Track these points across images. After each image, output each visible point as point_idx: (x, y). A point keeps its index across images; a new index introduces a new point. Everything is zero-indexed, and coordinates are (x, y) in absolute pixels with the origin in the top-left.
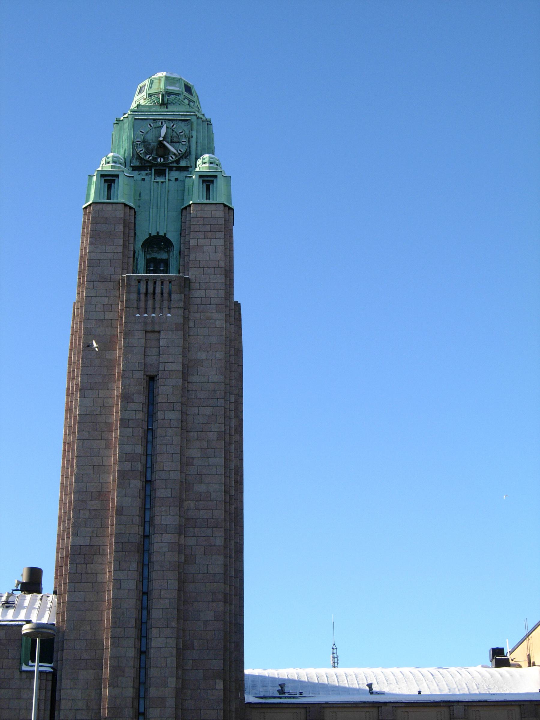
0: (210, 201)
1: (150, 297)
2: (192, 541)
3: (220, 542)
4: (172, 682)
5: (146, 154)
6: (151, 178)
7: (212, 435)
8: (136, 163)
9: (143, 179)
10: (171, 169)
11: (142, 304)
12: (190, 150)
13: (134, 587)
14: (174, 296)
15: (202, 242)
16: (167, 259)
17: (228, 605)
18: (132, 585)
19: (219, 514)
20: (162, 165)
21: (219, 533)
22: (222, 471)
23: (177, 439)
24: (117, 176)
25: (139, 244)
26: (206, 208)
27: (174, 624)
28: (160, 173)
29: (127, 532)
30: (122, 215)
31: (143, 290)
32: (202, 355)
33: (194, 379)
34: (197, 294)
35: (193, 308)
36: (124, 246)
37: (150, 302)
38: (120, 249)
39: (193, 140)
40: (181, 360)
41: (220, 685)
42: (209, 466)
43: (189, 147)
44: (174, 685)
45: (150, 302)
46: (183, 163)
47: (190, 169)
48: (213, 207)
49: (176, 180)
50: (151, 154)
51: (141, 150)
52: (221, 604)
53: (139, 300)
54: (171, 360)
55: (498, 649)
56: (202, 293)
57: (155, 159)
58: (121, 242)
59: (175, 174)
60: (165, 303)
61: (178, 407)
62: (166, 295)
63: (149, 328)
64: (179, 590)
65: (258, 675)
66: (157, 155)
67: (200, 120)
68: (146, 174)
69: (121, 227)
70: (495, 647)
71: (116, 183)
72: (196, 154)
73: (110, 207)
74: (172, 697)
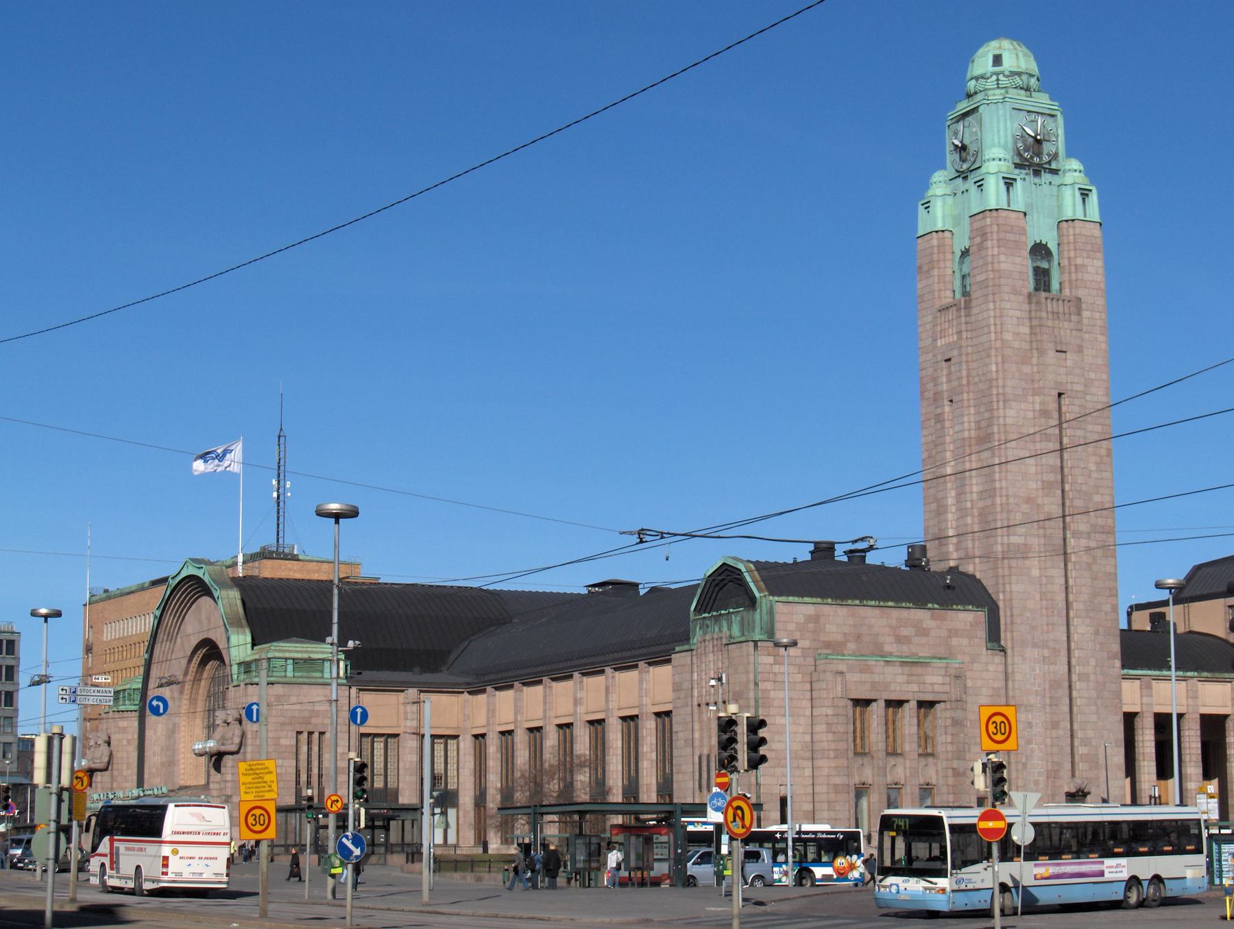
8: (1017, 161)
16: (990, 909)
20: (1038, 165)
43: (1057, 148)
50: (1028, 151)
57: (1032, 158)
65: (1225, 754)
66: (1033, 153)
74: (821, 741)
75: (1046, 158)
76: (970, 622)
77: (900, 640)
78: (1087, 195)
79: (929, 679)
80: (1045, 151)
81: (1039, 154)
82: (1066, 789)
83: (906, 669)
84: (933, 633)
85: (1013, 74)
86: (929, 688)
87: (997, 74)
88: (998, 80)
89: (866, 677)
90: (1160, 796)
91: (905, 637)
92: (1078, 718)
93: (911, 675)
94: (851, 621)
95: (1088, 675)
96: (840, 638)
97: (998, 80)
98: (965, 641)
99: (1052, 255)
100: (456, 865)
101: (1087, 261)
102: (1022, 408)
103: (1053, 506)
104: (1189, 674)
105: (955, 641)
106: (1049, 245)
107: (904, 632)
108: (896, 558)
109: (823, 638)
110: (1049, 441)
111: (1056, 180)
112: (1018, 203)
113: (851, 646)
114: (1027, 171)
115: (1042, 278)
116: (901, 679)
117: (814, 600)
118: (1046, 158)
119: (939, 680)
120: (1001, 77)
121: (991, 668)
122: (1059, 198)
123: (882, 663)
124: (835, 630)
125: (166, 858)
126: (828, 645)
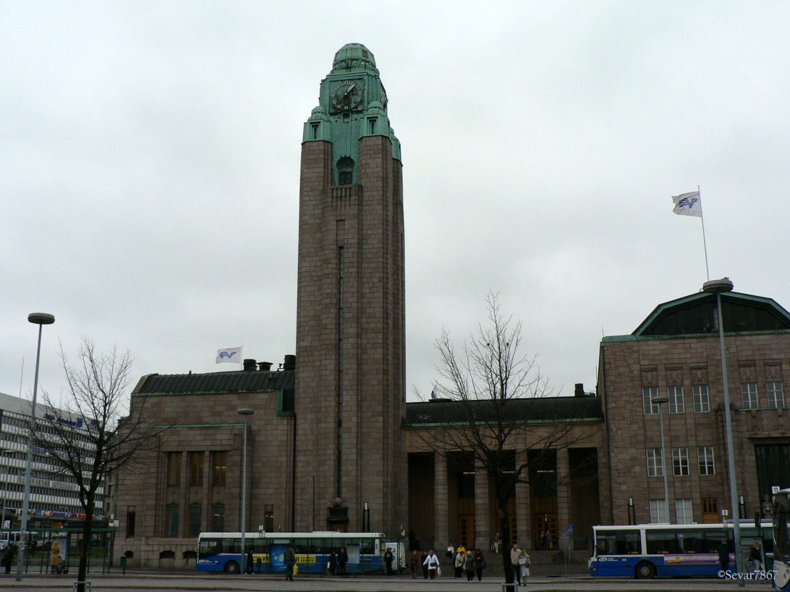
0: (374, 135)
1: (339, 199)
2: (365, 341)
3: (380, 341)
4: (354, 419)
5: (338, 104)
6: (340, 119)
7: (376, 280)
8: (332, 111)
9: (336, 121)
10: (353, 113)
11: (334, 204)
12: (364, 100)
14: (352, 198)
15: (369, 161)
17: (386, 376)
18: (333, 367)
19: (380, 325)
20: (347, 110)
21: (380, 336)
22: (381, 300)
23: (355, 284)
24: (320, 122)
25: (335, 163)
26: (372, 139)
27: (355, 388)
29: (329, 338)
30: (323, 148)
31: (335, 195)
32: (370, 232)
34: (366, 194)
35: (364, 203)
36: (324, 168)
38: (322, 170)
39: (366, 92)
41: (381, 419)
42: (374, 297)
43: (363, 97)
44: (355, 421)
46: (360, 108)
47: (364, 112)
48: (375, 138)
49: (356, 119)
51: (335, 102)
52: (381, 376)
53: (332, 202)
54: (351, 237)
55: (579, 384)
57: (343, 107)
58: (322, 165)
59: (355, 116)
60: (347, 202)
62: (348, 198)
63: (339, 219)
64: (358, 369)
66: (344, 104)
67: (370, 77)
68: (338, 118)
69: (322, 156)
70: (577, 383)
72: (368, 100)
73: (316, 144)
75: (353, 105)
76: (266, 399)
77: (214, 414)
79: (219, 437)
80: (353, 101)
81: (349, 104)
83: (203, 432)
86: (218, 443)
90: (368, 510)
93: (206, 435)
99: (354, 162)
100: (68, 564)
107: (218, 409)
115: (346, 177)
116: (199, 438)
118: (353, 105)
119: (227, 437)
122: (359, 127)
123: (187, 429)
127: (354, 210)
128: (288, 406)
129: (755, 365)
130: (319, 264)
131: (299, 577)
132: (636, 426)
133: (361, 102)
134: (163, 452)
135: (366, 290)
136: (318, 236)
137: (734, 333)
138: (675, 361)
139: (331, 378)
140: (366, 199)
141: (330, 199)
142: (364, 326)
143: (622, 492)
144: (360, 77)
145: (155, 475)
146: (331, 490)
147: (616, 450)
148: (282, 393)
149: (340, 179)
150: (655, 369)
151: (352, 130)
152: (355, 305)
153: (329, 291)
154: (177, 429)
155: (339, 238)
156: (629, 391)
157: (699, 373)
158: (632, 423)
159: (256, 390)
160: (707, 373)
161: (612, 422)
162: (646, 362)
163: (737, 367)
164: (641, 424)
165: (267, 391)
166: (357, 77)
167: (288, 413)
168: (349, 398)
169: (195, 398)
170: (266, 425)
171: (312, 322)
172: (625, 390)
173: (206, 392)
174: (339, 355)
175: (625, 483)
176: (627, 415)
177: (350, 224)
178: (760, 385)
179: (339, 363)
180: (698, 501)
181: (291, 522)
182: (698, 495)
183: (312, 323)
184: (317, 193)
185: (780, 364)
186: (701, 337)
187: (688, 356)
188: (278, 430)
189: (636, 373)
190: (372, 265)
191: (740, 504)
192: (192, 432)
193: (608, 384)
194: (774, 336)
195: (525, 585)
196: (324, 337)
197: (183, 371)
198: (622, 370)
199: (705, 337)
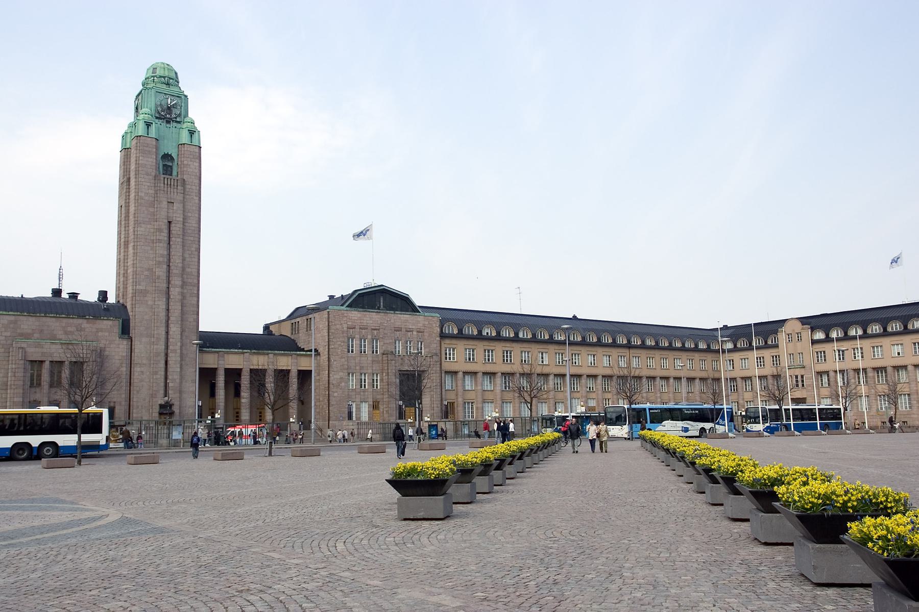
2: (185, 291)
4: (179, 344)
11: (166, 189)
13: (164, 307)
15: (190, 163)
20: (169, 118)
23: (181, 250)
27: (180, 323)
28: (168, 122)
33: (187, 224)
37: (169, 189)
38: (155, 161)
40: (182, 216)
43: (181, 112)
44: (180, 345)
45: (169, 189)
49: (176, 127)
50: (164, 112)
56: (189, 187)
59: (175, 124)
61: (181, 237)
62: (175, 186)
71: (720, 479)
75: (173, 116)
76: (110, 325)
77: (66, 333)
78: (193, 133)
80: (174, 113)
81: (170, 114)
82: (160, 403)
84: (87, 330)
85: (161, 77)
87: (154, 77)
88: (154, 80)
89: (40, 350)
91: (71, 332)
92: (170, 370)
94: (37, 323)
95: (176, 350)
96: (30, 331)
97: (154, 80)
98: (107, 334)
101: (190, 163)
102: (148, 227)
103: (161, 273)
104: (245, 351)
105: (100, 334)
106: (172, 155)
107: (69, 329)
108: (93, 298)
109: (19, 331)
110: (161, 243)
111: (178, 126)
112: (152, 133)
113: (36, 335)
114: (163, 121)
115: (168, 170)
117: (16, 313)
118: (173, 116)
120: (155, 78)
121: (121, 346)
124: (27, 328)
125: (643, 398)
126: (21, 335)
127: (180, 197)
128: (125, 330)
129: (401, 331)
130: (152, 230)
131: (169, 449)
132: (343, 359)
133: (180, 115)
134: (27, 361)
135: (187, 256)
136: (151, 210)
137: (393, 312)
138: (365, 324)
139: (163, 314)
140: (188, 190)
141: (162, 185)
142: (185, 280)
143: (335, 397)
144: (179, 96)
145: (22, 379)
146: (162, 392)
147: (333, 373)
148: (121, 321)
149: (163, 170)
150: (354, 328)
151: (173, 135)
152: (180, 265)
153: (161, 252)
154: (41, 343)
155: (171, 215)
156: (341, 339)
157: (375, 332)
158: (342, 358)
159: (100, 317)
160: (379, 332)
161: (332, 356)
162: (350, 323)
163: (393, 331)
164: (346, 359)
165: (109, 318)
166: (177, 95)
167: (126, 336)
168: (175, 330)
169: (48, 319)
170: (110, 344)
171: (147, 272)
172: (339, 339)
173: (58, 316)
174: (168, 298)
175: (336, 392)
176: (339, 353)
177: (177, 206)
178: (403, 341)
179: (168, 304)
180: (371, 403)
181: (128, 414)
182: (371, 400)
183: (146, 273)
184: (151, 177)
185: (412, 331)
186: (377, 312)
187: (371, 322)
188: (117, 349)
189: (345, 329)
190: (192, 239)
191: (199, 406)
192: (54, 346)
193: (330, 334)
194: (411, 316)
195: (446, 439)
196: (157, 284)
197: (17, 295)
198: (338, 326)
199: (380, 312)
